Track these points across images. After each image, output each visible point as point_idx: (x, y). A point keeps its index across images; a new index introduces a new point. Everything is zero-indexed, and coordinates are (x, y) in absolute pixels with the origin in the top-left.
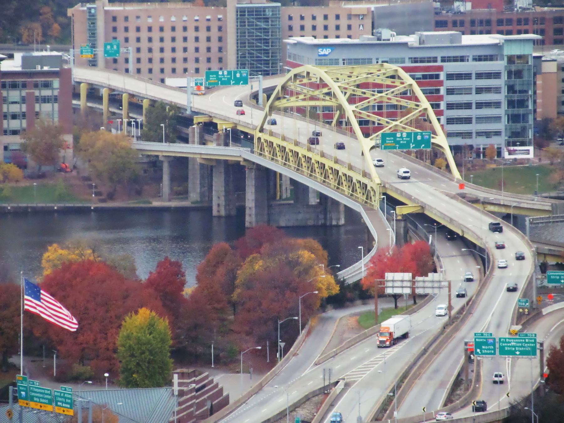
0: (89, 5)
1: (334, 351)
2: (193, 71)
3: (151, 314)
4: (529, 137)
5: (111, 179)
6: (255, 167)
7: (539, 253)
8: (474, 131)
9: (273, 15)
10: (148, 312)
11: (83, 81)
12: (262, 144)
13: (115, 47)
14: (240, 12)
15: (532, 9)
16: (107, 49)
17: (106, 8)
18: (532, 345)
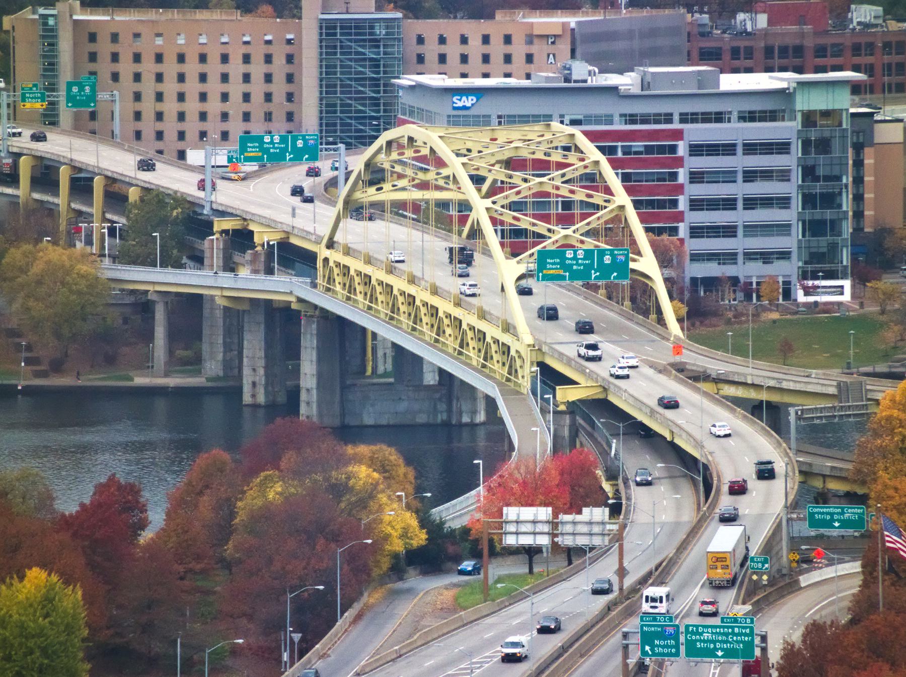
0: (42, 11)
1: (396, 650)
2: (217, 136)
3: (49, 579)
4: (842, 263)
5: (58, 335)
6: (317, 313)
7: (806, 474)
8: (740, 251)
9: (387, 34)
10: (43, 575)
11: (25, 152)
12: (331, 270)
13: (87, 89)
15: (882, 26)
16: (72, 93)
17: (75, 17)
18: (746, 639)
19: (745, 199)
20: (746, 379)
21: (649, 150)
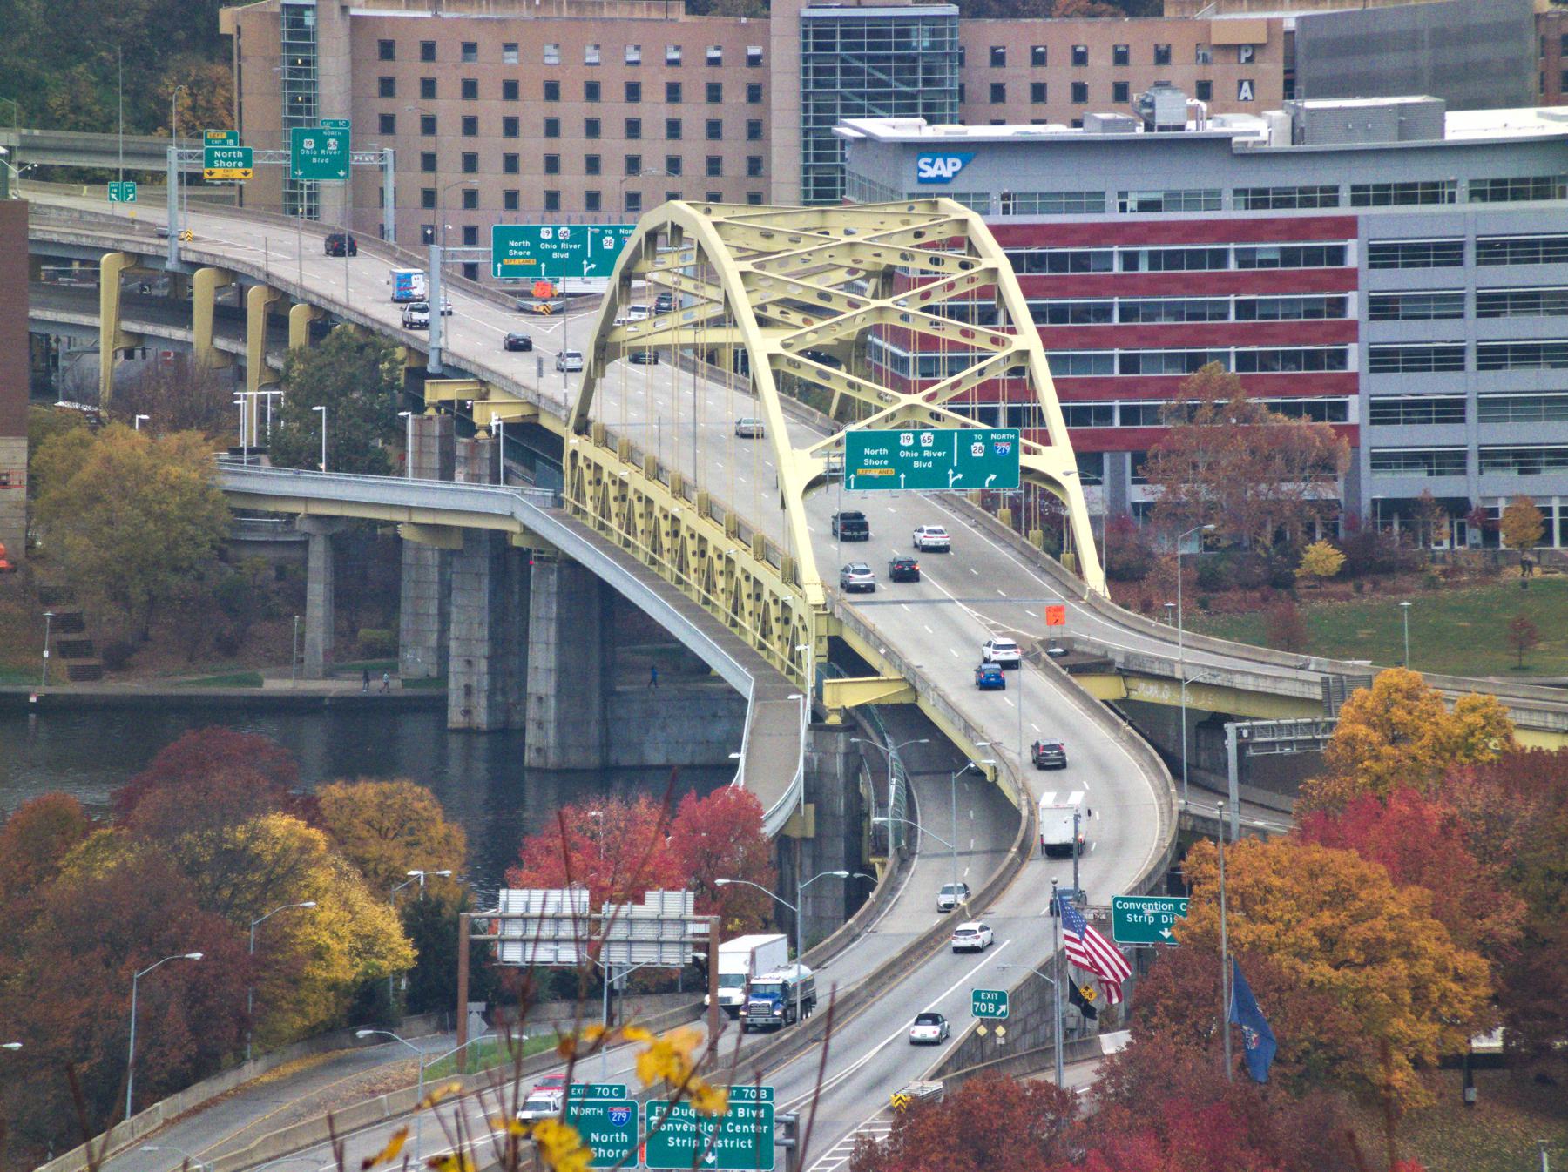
8: (1472, 449)
9: (933, 46)
11: (206, 260)
14: (817, 34)
16: (302, 152)
19: (1480, 350)
20: (1172, 671)
21: (1289, 257)
